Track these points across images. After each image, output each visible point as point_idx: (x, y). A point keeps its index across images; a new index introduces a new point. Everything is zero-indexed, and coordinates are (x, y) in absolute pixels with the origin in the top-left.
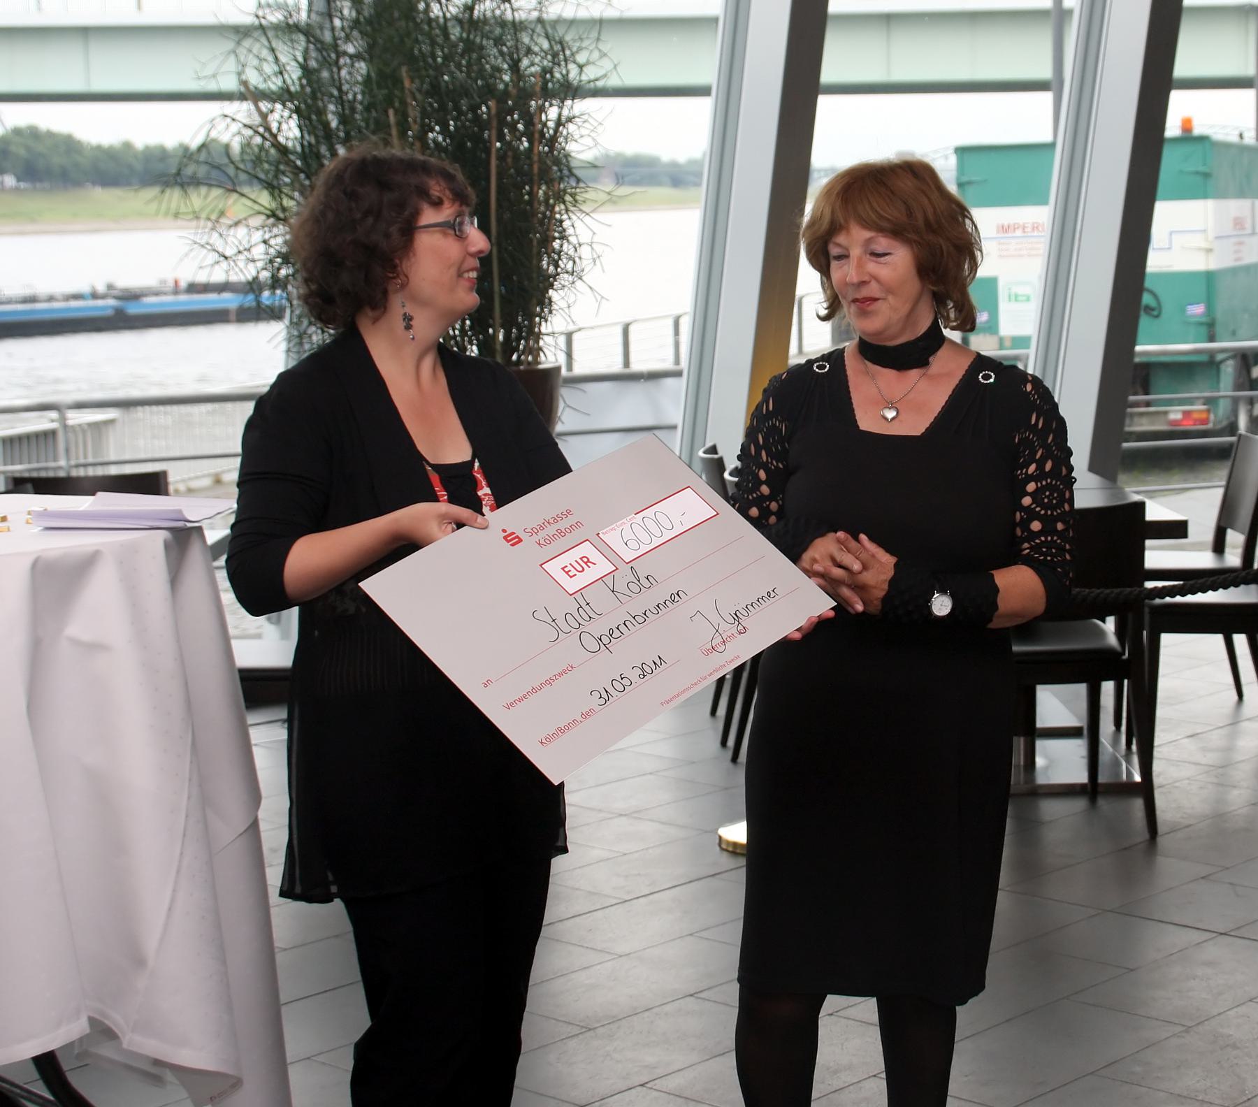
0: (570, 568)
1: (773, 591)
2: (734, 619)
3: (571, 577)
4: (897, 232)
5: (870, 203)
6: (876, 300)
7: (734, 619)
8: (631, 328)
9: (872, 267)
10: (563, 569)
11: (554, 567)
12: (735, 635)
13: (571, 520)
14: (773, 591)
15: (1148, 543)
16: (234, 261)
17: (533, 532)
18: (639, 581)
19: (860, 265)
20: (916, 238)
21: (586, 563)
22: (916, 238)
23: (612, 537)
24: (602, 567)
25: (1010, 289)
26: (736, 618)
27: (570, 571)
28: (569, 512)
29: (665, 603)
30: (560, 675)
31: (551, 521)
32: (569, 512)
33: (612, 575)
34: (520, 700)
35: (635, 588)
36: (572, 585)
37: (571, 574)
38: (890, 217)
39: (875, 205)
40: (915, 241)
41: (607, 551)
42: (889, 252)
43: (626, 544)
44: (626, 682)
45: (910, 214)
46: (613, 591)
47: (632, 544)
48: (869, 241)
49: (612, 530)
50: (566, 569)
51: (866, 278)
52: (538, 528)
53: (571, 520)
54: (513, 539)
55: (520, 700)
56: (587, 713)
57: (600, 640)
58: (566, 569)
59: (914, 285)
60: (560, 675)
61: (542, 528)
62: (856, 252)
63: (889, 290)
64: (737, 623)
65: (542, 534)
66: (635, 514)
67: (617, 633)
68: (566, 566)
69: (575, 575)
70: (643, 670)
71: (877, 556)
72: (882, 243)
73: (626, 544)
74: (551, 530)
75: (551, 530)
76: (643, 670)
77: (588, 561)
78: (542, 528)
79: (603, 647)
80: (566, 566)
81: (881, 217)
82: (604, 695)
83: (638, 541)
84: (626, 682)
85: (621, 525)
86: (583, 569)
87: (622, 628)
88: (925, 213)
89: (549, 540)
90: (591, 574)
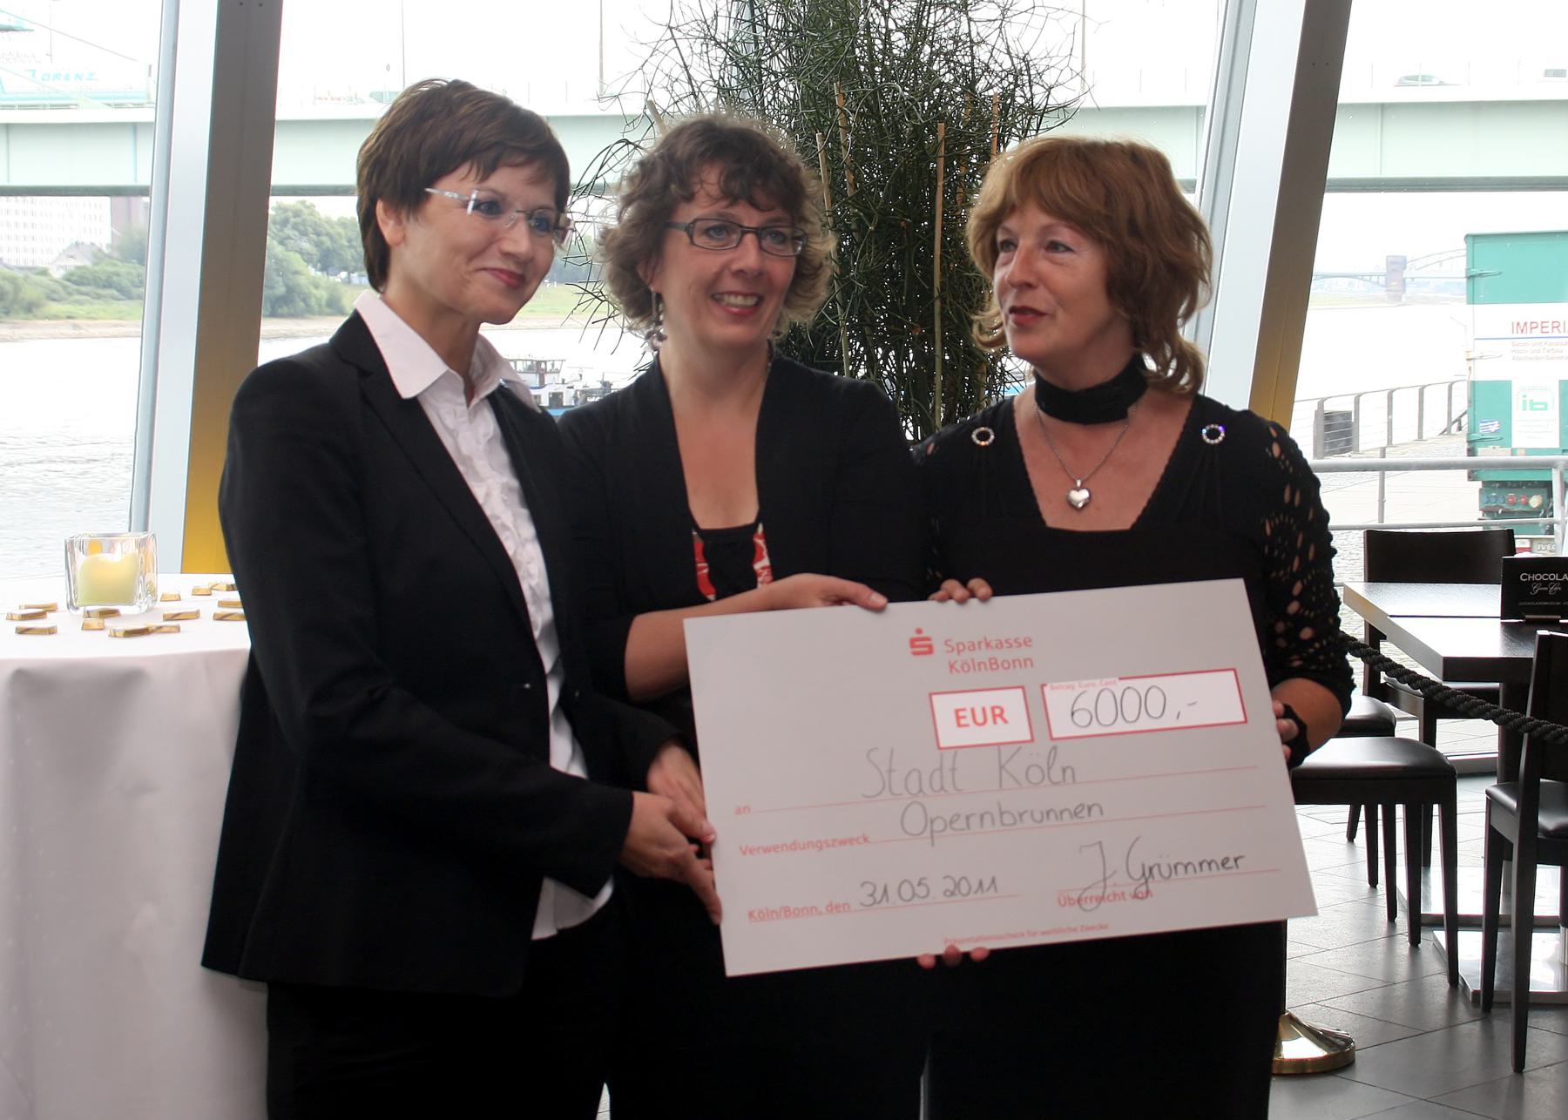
0: (968, 714)
1: (1236, 860)
2: (1144, 874)
3: (959, 725)
4: (1083, 223)
5: (1057, 177)
6: (1040, 314)
7: (1144, 874)
8: (1454, 386)
9: (1043, 266)
10: (957, 711)
11: (945, 706)
12: (1127, 896)
13: (1023, 653)
14: (1236, 860)
15: (1538, 865)
16: (711, 77)
17: (959, 648)
18: (1049, 768)
19: (1027, 261)
20: (1109, 236)
21: (994, 716)
22: (1109, 236)
23: (1059, 699)
24: (1016, 728)
25: (1525, 396)
26: (1147, 873)
27: (964, 717)
28: (1027, 642)
29: (1061, 813)
30: (843, 842)
31: (993, 644)
32: (1027, 642)
33: (1018, 745)
34: (767, 850)
35: (1035, 775)
36: (950, 735)
37: (963, 722)
38: (1078, 200)
39: (1062, 179)
40: (1109, 242)
41: (1037, 712)
42: (1073, 248)
43: (1073, 714)
44: (921, 891)
45: (1109, 200)
46: (1001, 767)
47: (1082, 718)
48: (1046, 229)
49: (1068, 687)
50: (961, 714)
51: (1032, 280)
52: (967, 645)
53: (1023, 653)
54: (921, 645)
55: (767, 850)
56: (837, 907)
57: (932, 822)
58: (961, 714)
59: (1098, 307)
60: (843, 842)
61: (972, 647)
62: (1026, 242)
63: (1062, 301)
64: (1143, 880)
65: (966, 655)
66: (1121, 679)
67: (961, 824)
68: (963, 710)
69: (1020, 748)
70: (957, 885)
71: (51, 272)
72: (1065, 235)
73: (1073, 714)
74: (983, 655)
75: (983, 655)
76: (957, 885)
77: (1001, 715)
78: (972, 647)
79: (927, 833)
80: (963, 710)
81: (1066, 197)
82: (878, 896)
83: (1094, 716)
84: (921, 891)
85: (1088, 686)
86: (985, 722)
87: (975, 821)
88: (1132, 211)
89: (967, 667)
90: (993, 733)
